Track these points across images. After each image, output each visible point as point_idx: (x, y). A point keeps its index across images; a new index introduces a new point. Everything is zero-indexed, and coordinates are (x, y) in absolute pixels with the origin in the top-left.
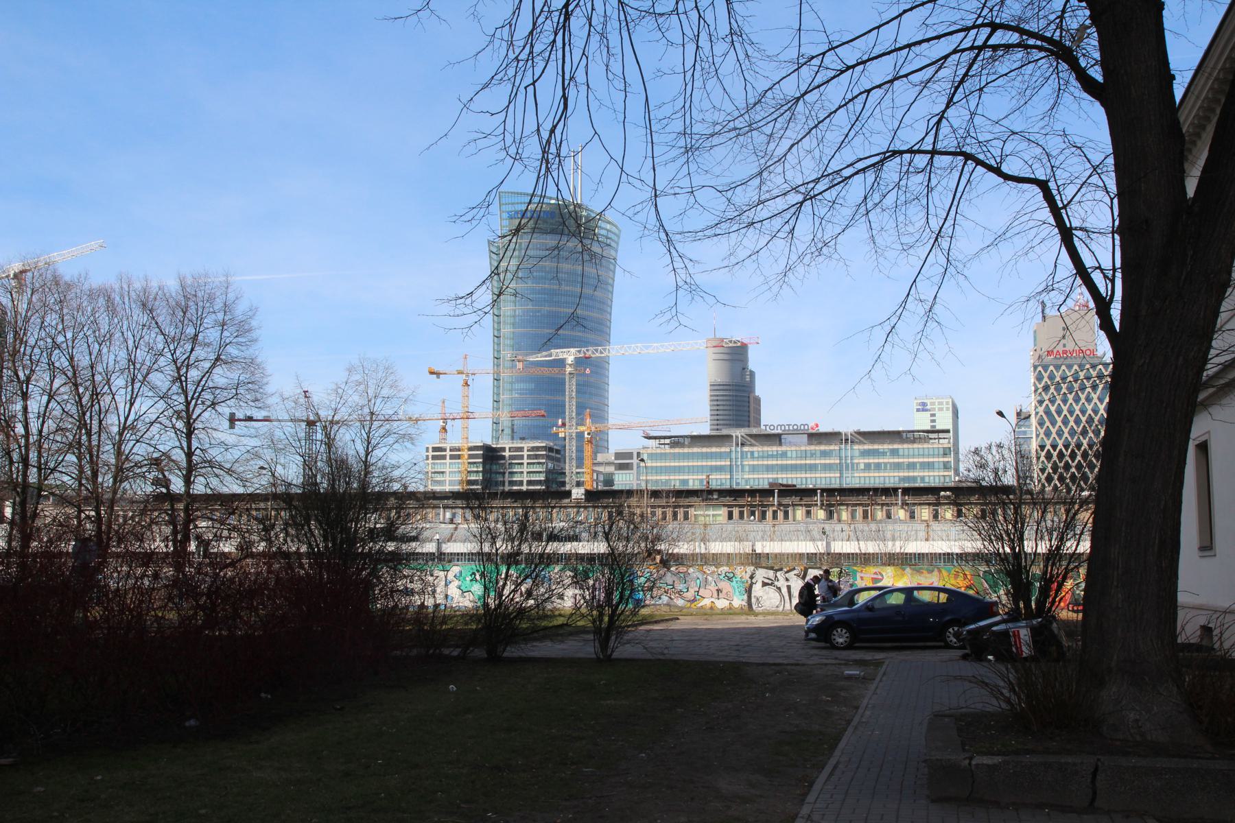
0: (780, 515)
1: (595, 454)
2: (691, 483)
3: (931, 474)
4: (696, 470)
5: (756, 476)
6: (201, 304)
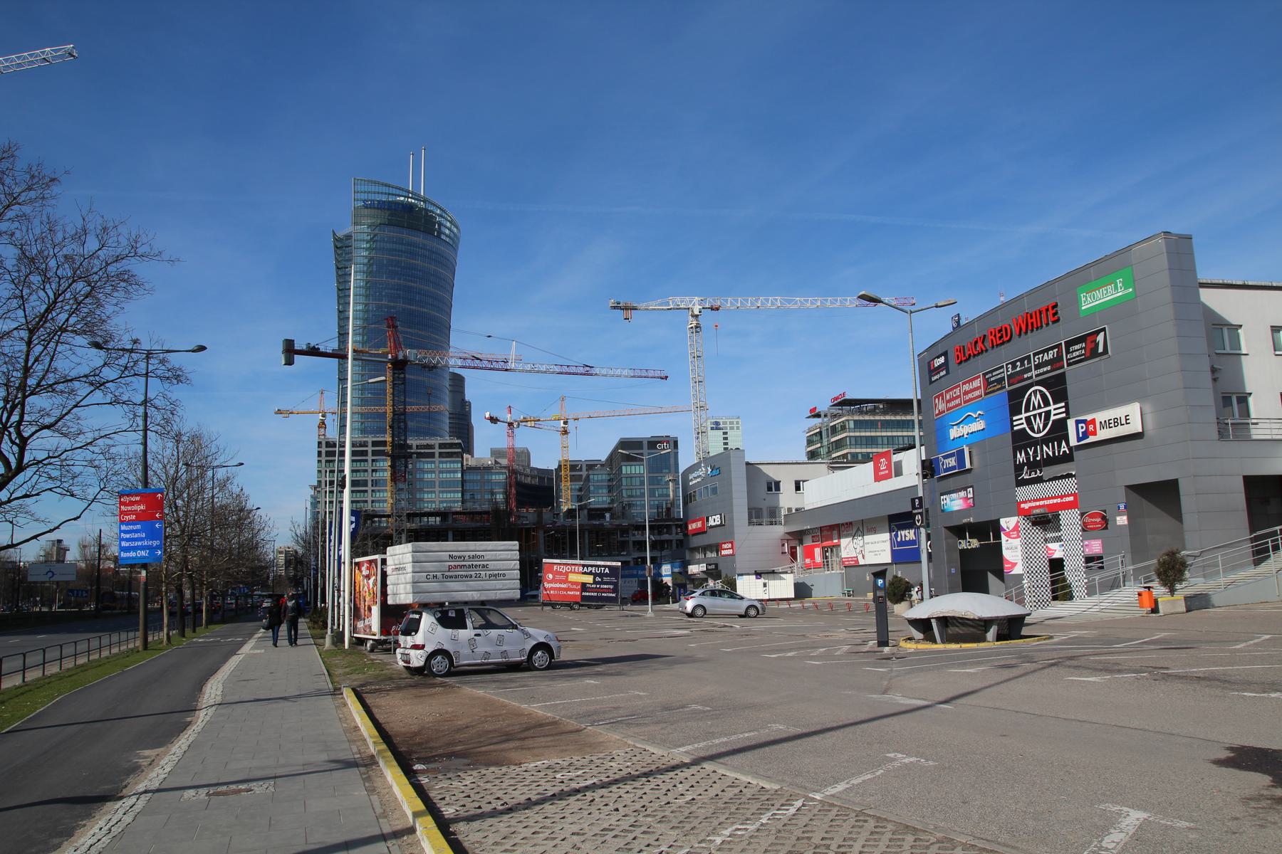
4: (864, 442)
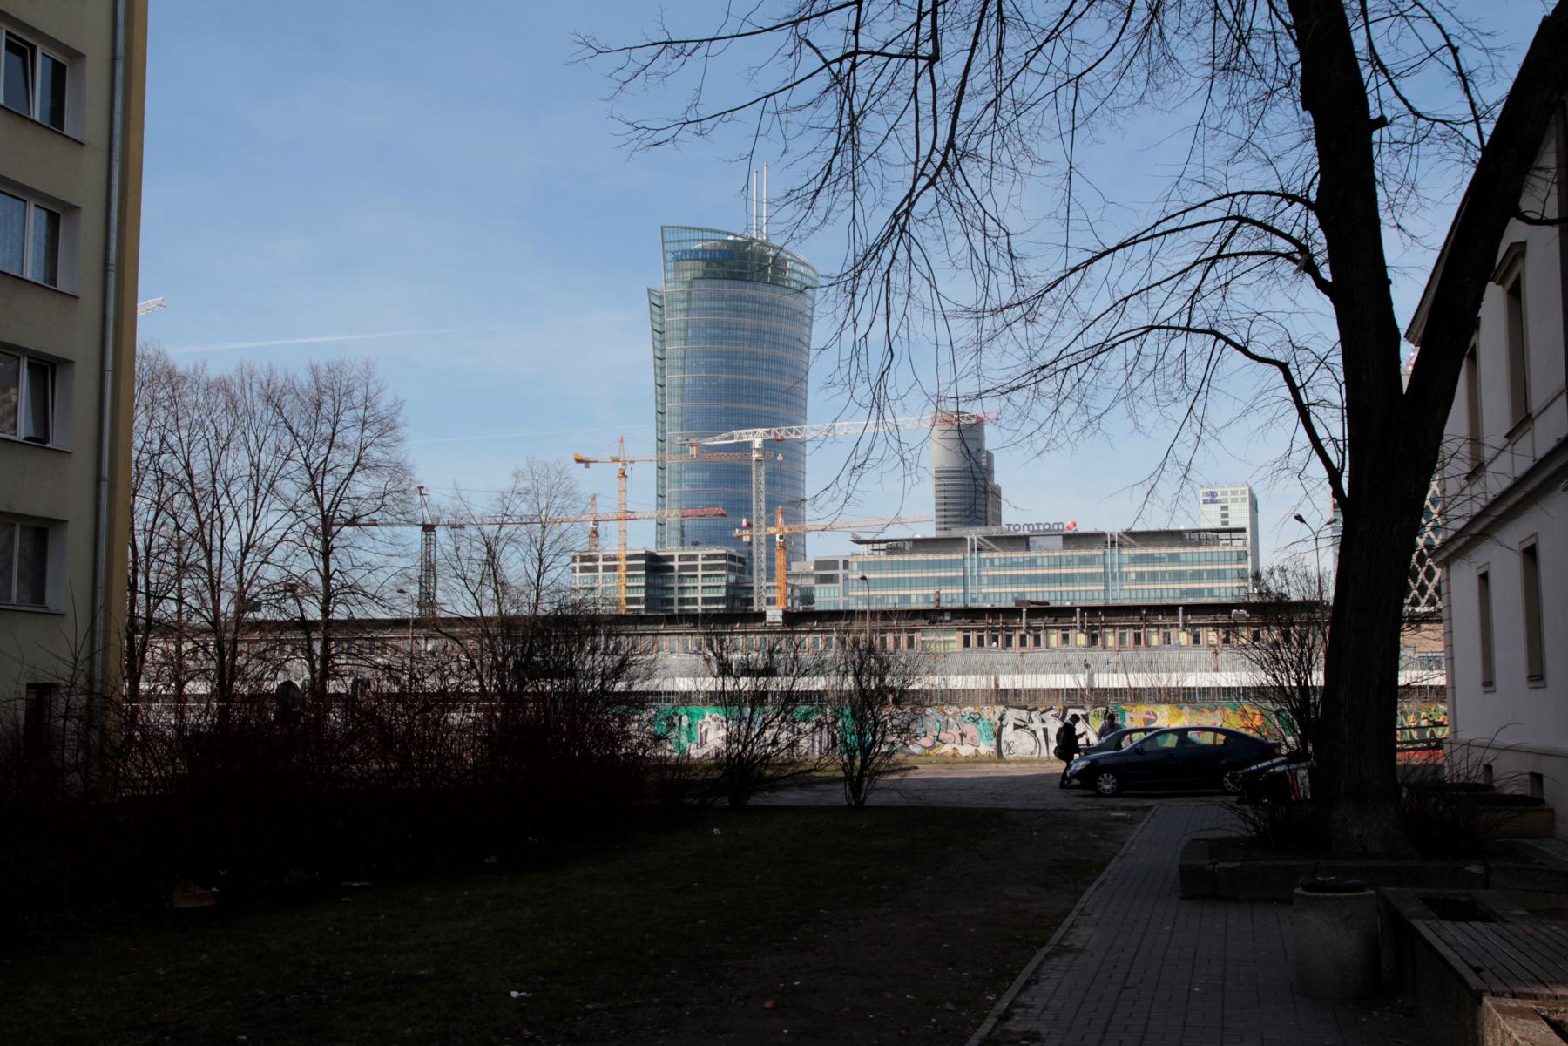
0: (1030, 640)
1: (789, 563)
2: (913, 599)
3: (1222, 585)
5: (997, 590)
6: (337, 398)
